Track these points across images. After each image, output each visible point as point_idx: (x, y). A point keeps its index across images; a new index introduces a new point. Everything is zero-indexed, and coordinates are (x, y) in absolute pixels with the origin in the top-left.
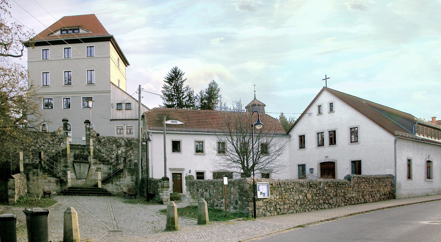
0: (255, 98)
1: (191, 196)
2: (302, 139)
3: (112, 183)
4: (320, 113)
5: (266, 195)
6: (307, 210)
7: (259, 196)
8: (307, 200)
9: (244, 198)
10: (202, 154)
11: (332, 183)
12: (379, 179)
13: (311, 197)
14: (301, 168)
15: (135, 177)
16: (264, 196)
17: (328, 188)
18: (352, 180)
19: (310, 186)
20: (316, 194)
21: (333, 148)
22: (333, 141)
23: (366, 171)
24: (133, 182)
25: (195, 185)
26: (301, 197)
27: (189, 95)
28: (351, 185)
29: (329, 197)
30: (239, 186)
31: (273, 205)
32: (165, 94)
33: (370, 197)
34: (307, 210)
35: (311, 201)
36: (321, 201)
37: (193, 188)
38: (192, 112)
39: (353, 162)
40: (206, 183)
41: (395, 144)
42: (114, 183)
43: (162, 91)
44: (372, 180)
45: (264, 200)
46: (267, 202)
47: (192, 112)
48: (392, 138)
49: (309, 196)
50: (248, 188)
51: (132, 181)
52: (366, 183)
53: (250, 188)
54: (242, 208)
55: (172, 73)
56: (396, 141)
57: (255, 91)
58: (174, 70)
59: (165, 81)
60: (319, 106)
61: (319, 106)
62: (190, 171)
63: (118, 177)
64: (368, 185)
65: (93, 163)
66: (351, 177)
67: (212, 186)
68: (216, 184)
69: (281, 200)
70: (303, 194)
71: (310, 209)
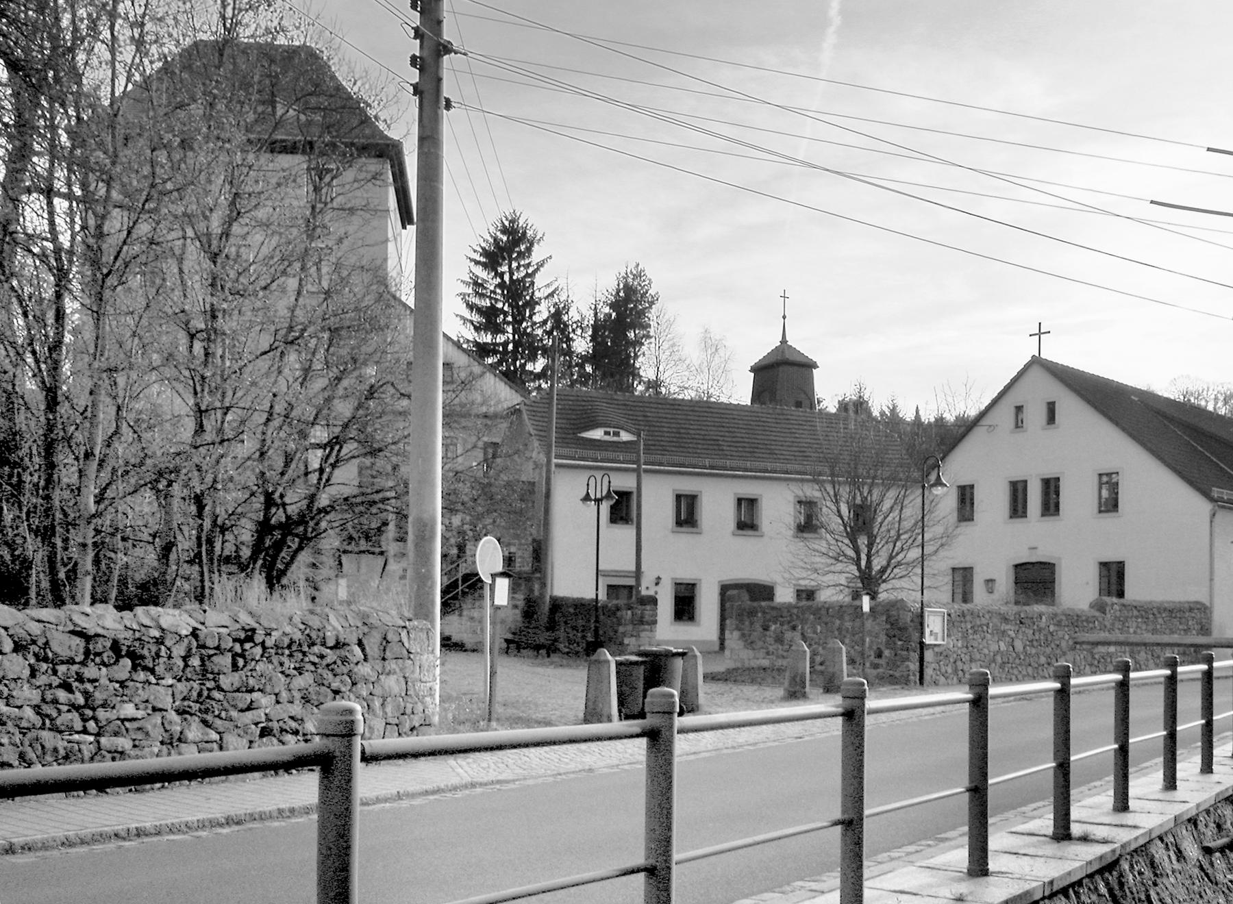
0: (784, 341)
1: (743, 644)
2: (966, 496)
3: (460, 615)
4: (1019, 424)
5: (940, 636)
6: (1014, 678)
7: (928, 640)
8: (1014, 655)
9: (900, 643)
10: (694, 530)
11: (1064, 618)
12: (1171, 611)
13: (1022, 649)
14: (958, 577)
15: (522, 597)
16: (936, 639)
17: (1056, 628)
18: (1108, 609)
19: (1021, 623)
20: (1032, 641)
21: (1050, 523)
22: (1051, 506)
23: (1135, 591)
24: (518, 611)
25: (760, 615)
26: (1003, 647)
27: (557, 316)
28: (1107, 623)
29: (1058, 652)
30: (889, 617)
31: (952, 660)
32: (471, 307)
33: (1150, 657)
34: (1014, 678)
35: (1022, 657)
36: (1043, 660)
37: (752, 623)
38: (655, 406)
39: (1104, 565)
40: (795, 611)
41: (1211, 522)
42: (465, 613)
43: (464, 296)
44: (1153, 614)
45: (936, 649)
46: (941, 653)
47: (655, 406)
48: (1202, 507)
49: (1019, 645)
50: (909, 619)
51: (516, 607)
52: (1140, 620)
53: (912, 621)
54: (893, 664)
55: (498, 233)
56: (1214, 515)
57: (784, 317)
58: (507, 223)
59: (472, 260)
60: (1019, 409)
61: (1019, 409)
62: (659, 578)
63: (476, 595)
64: (1144, 627)
65: (395, 555)
66: (1107, 604)
67: (812, 617)
68: (823, 612)
69: (964, 650)
70: (1007, 639)
71: (1020, 677)
